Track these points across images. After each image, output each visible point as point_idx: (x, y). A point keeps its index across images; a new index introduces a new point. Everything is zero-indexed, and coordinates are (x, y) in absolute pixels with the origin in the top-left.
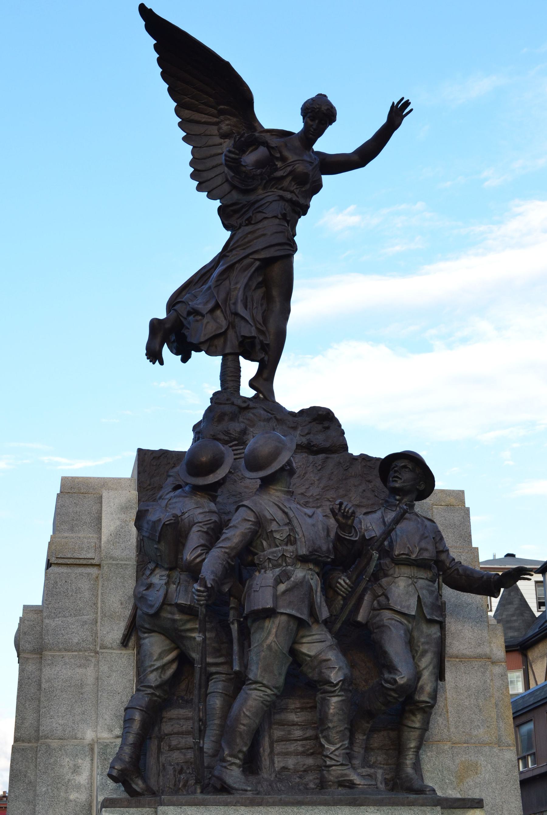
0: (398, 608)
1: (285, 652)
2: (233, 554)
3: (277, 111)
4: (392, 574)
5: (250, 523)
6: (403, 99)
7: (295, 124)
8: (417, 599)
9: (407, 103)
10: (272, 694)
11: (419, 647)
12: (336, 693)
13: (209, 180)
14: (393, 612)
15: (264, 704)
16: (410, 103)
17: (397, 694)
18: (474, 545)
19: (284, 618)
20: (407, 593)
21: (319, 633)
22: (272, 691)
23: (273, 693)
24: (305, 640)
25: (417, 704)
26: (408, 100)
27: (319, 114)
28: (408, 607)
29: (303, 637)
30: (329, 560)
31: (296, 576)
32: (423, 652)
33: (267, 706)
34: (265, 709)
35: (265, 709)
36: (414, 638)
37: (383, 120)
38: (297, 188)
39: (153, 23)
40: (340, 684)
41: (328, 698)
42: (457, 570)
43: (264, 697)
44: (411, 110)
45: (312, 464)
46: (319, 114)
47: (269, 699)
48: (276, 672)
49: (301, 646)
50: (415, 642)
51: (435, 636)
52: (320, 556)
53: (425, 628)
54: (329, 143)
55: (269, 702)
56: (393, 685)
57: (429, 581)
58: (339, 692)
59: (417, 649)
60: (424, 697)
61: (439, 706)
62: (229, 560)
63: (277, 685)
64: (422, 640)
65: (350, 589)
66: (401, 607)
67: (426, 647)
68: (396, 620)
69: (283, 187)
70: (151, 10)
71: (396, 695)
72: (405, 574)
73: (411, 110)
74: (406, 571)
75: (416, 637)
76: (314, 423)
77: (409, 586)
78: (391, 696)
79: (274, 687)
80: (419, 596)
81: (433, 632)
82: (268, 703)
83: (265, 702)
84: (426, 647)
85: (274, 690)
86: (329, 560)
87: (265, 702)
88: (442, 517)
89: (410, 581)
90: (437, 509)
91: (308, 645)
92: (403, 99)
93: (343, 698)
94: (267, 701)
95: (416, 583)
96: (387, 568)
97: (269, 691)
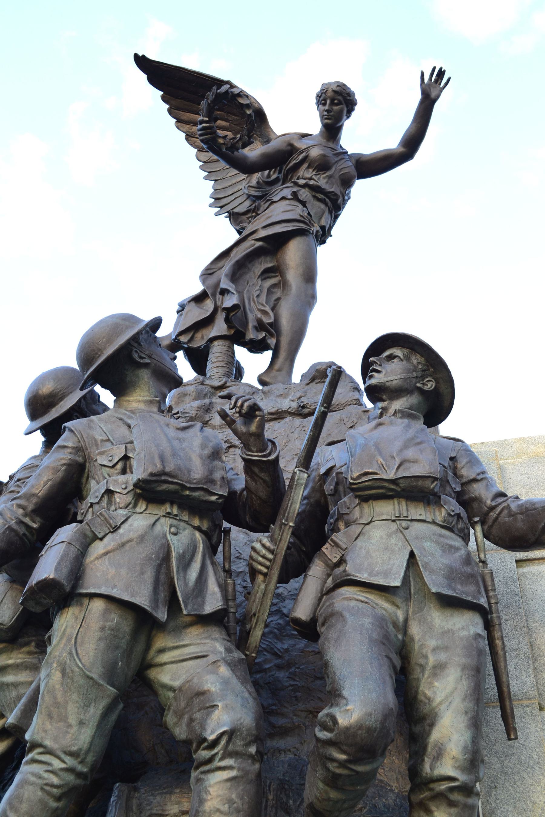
0: (364, 577)
1: (95, 676)
2: (30, 507)
3: (292, 116)
4: (356, 520)
5: (69, 450)
6: (434, 69)
7: (312, 124)
8: (407, 557)
9: (441, 73)
10: (62, 769)
11: (426, 657)
12: (217, 763)
13: (229, 203)
14: (362, 589)
15: (49, 793)
16: (444, 71)
17: (344, 752)
18: (141, 55)
19: (98, 605)
20: (386, 549)
21: (198, 642)
22: (64, 762)
23: (63, 766)
24: (165, 657)
25: (432, 786)
26: (441, 68)
27: (337, 103)
28: (386, 574)
29: (162, 651)
30: (214, 498)
31: (131, 525)
32: (435, 667)
33: (58, 799)
34: (54, 804)
35: (54, 804)
36: (412, 639)
37: (418, 96)
38: (316, 175)
39: (157, 73)
40: (223, 742)
41: (202, 776)
42: (508, 507)
43: (46, 775)
44: (449, 80)
45: (299, 429)
46: (337, 103)
47: (55, 780)
48: (73, 719)
49: (158, 669)
50: (416, 647)
51: (464, 633)
52: (184, 487)
53: (440, 620)
54: (360, 137)
55: (57, 787)
56: (330, 730)
57: (442, 527)
58: (221, 759)
59: (422, 661)
60: (447, 768)
61: (534, 803)
62: (27, 520)
63: (74, 749)
64: (432, 643)
65: (270, 556)
66: (370, 574)
67: (443, 656)
68: (357, 600)
69: (299, 176)
70: (143, 56)
71: (343, 757)
72: (382, 514)
73: (449, 80)
74: (386, 509)
75: (417, 638)
76: (313, 384)
77: (390, 535)
78: (333, 760)
79: (65, 753)
80: (412, 555)
81: (458, 626)
82: (55, 791)
83: (48, 788)
84: (443, 656)
85: (68, 759)
86: (214, 498)
87: (48, 788)
88: (522, 475)
89: (394, 527)
90: (513, 464)
91: (174, 666)
92: (434, 69)
93: (233, 773)
94: (52, 786)
95: (407, 528)
96: (347, 511)
97: (57, 764)
